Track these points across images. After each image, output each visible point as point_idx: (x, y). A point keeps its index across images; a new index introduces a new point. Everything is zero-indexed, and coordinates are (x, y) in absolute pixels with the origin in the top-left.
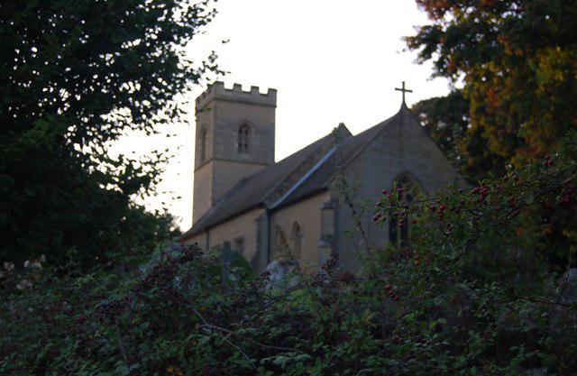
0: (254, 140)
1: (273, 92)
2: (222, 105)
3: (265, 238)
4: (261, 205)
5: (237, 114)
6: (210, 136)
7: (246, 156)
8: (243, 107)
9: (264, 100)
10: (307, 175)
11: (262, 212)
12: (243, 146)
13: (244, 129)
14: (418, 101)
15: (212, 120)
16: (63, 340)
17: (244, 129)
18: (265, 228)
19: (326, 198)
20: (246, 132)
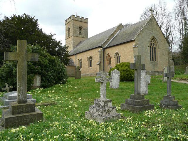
0: (83, 31)
1: (87, 19)
2: (75, 22)
3: (102, 57)
4: (100, 47)
5: (79, 24)
6: (71, 30)
7: (81, 36)
8: (80, 22)
9: (85, 21)
10: (108, 44)
11: (100, 49)
12: (80, 33)
13: (80, 28)
14: (10, 15)
15: (72, 25)
16: (63, 64)
17: (80, 28)
18: (102, 53)
19: (134, 44)
20: (80, 29)
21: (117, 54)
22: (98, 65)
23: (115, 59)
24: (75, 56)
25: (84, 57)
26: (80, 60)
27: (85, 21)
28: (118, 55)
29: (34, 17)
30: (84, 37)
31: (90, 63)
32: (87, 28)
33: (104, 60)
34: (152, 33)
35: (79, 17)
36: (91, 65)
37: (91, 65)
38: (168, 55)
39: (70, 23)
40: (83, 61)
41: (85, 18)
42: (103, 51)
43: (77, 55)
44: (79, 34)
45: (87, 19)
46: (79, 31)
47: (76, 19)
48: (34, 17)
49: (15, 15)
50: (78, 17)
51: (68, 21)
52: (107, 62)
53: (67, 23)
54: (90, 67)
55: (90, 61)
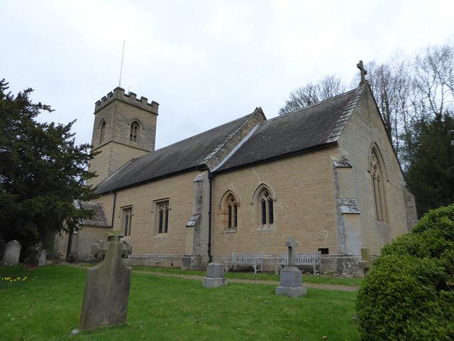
0: (141, 134)
1: (155, 105)
7: (135, 144)
9: (150, 108)
12: (134, 137)
13: (135, 124)
17: (135, 124)
21: (265, 190)
22: (193, 229)
23: (253, 209)
24: (110, 199)
25: (142, 199)
26: (128, 209)
27: (152, 109)
28: (267, 195)
29: (70, 125)
30: (145, 148)
31: (161, 219)
32: (155, 127)
33: (210, 213)
34: (371, 133)
35: (135, 95)
36: (163, 226)
37: (163, 226)
38: (406, 203)
39: (107, 108)
40: (134, 212)
41: (149, 102)
42: (208, 180)
43: (120, 194)
44: (131, 140)
45: (155, 105)
46: (132, 131)
47: (128, 99)
48: (70, 125)
49: (53, 124)
50: (132, 96)
51: (103, 105)
52: (221, 219)
53: (99, 107)
54: (160, 232)
55: (161, 213)
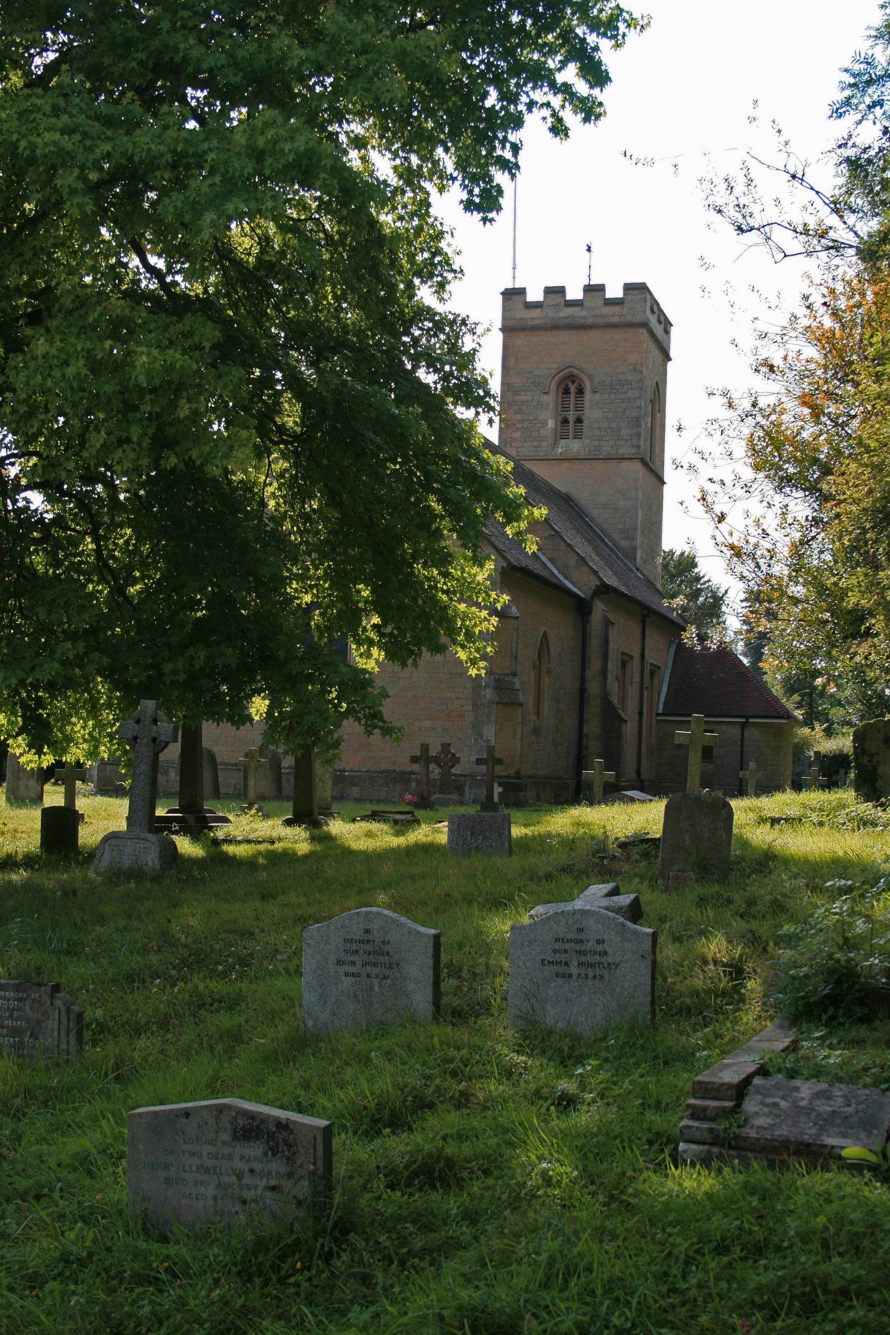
2: (520, 340)
50: (555, 299)
